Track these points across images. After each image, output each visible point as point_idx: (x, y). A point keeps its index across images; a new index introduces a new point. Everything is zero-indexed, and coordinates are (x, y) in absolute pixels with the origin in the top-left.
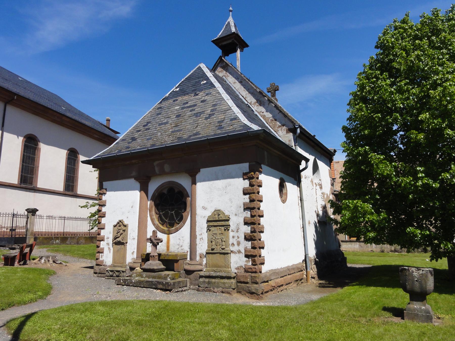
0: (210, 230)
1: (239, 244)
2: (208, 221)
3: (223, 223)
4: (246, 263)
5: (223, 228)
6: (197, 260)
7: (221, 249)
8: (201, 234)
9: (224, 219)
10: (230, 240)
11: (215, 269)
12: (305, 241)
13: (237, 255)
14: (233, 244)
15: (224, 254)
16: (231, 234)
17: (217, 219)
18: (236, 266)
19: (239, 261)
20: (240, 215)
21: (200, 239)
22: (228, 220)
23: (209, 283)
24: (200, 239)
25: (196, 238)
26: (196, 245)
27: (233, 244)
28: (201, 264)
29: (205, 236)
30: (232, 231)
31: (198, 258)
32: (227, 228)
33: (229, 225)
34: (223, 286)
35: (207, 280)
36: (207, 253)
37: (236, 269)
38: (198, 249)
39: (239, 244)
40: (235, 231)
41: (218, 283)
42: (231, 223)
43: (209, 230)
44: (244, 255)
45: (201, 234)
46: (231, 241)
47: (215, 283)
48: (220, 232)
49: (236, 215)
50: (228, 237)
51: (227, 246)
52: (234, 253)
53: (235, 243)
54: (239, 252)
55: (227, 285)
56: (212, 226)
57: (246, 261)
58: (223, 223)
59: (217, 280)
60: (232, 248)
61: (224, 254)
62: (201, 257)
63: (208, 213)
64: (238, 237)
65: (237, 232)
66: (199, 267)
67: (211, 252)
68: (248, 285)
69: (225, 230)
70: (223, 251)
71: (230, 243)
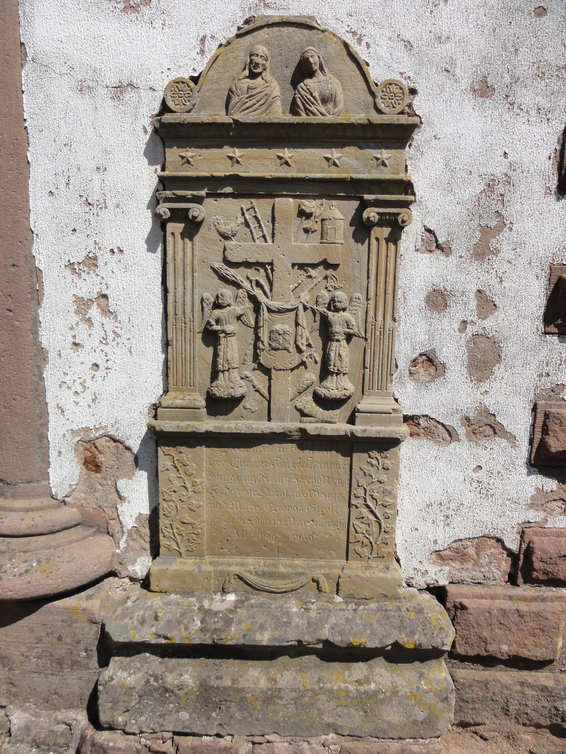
0: (192, 227)
1: (484, 359)
2: (169, 133)
3: (351, 162)
4: (534, 516)
5: (340, 212)
6: (59, 491)
7: (307, 402)
8: (91, 261)
9: (359, 116)
10: (403, 328)
11: (250, 565)
12: (165, 326)
13: (462, 449)
14: (429, 362)
15: (348, 445)
16: (417, 270)
17: (279, 114)
18: (444, 538)
19: (469, 497)
20: (526, 97)
21: (82, 305)
22: (398, 135)
23: (208, 698)
24: (82, 305)
25: (37, 296)
26: (41, 355)
27: (429, 362)
28: (98, 523)
29: (136, 280)
30: (435, 244)
31: (64, 471)
32: (381, 207)
33: (407, 187)
34: (354, 719)
35: (187, 674)
36: (158, 438)
37: (440, 556)
38: (53, 395)
39: (484, 359)
40: (461, 247)
41: (303, 699)
42: (422, 164)
43: (176, 211)
44: (523, 450)
45: (91, 261)
46: (412, 331)
47: (270, 697)
48: (308, 249)
49: (483, 89)
50: (383, 292)
51: (376, 371)
52: (429, 433)
53: (452, 352)
54: (485, 426)
55: (392, 715)
56: (214, 186)
57: (539, 501)
58: (351, 162)
59: (287, 675)
60: (411, 396)
61: (348, 445)
62: (92, 464)
63: (167, 51)
64: (486, 304)
65: (482, 252)
66: (91, 554)
67: (210, 424)
68: (542, 677)
69: (361, 229)
70: (337, 425)
71: (404, 351)
